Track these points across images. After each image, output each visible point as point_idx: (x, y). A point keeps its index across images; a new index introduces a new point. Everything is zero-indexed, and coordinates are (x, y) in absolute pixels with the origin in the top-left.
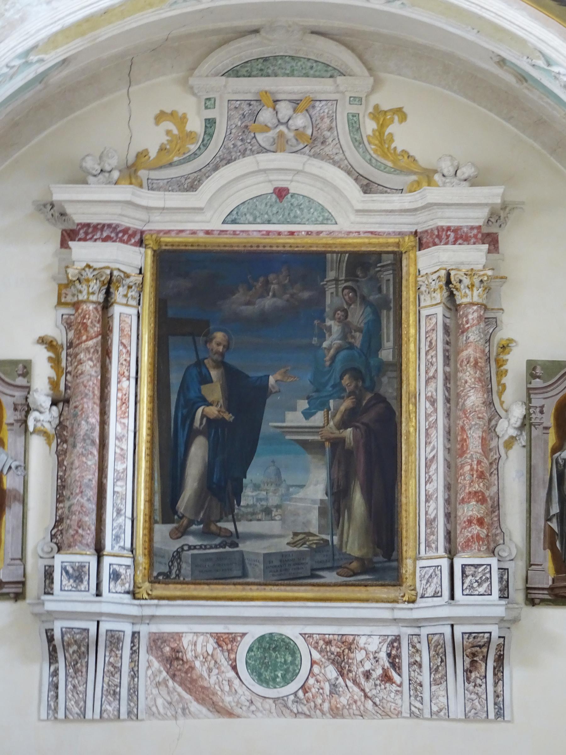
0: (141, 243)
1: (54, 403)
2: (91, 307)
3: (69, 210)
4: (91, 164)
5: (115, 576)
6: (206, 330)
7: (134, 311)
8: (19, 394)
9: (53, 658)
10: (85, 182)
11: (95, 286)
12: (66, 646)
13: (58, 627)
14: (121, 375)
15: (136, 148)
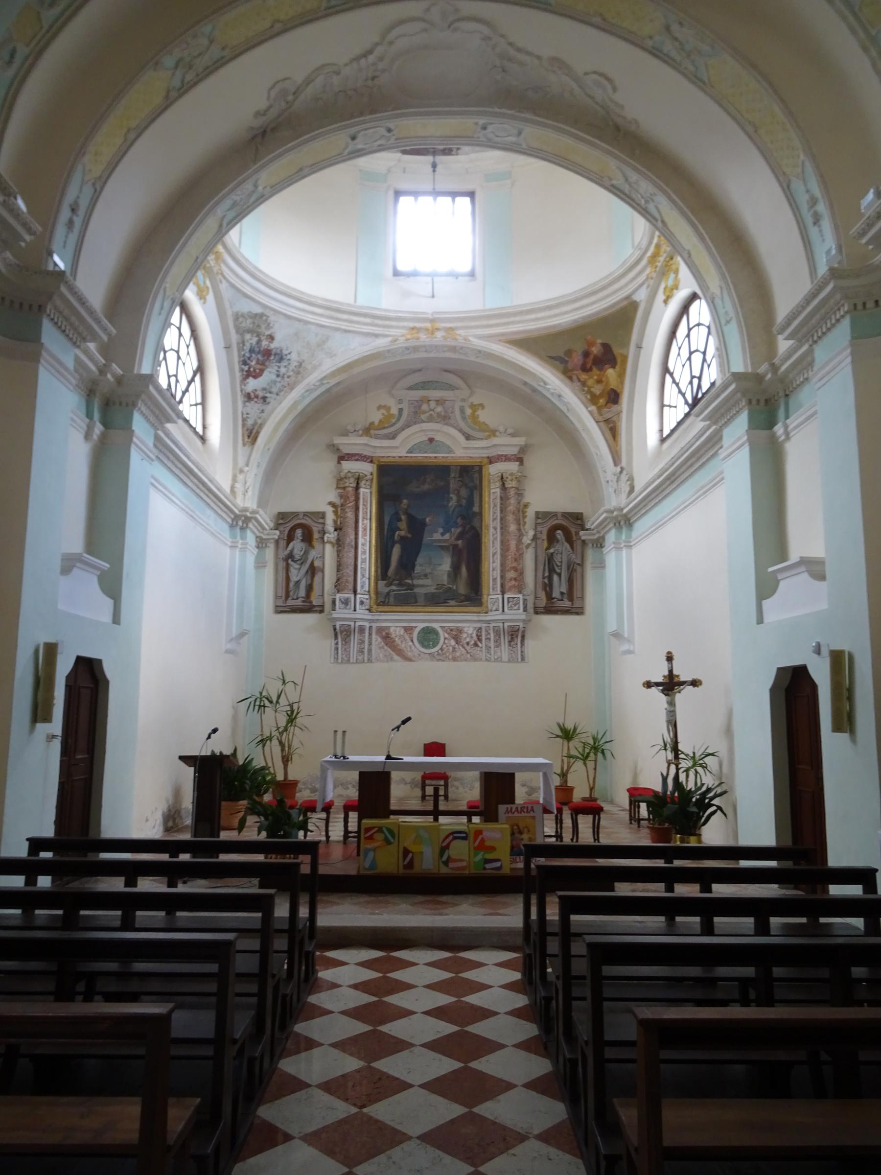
1: (336, 530)
2: (351, 489)
3: (341, 447)
4: (350, 428)
5: (362, 603)
7: (368, 491)
9: (336, 637)
10: (347, 435)
11: (352, 480)
13: (338, 624)
14: (364, 518)
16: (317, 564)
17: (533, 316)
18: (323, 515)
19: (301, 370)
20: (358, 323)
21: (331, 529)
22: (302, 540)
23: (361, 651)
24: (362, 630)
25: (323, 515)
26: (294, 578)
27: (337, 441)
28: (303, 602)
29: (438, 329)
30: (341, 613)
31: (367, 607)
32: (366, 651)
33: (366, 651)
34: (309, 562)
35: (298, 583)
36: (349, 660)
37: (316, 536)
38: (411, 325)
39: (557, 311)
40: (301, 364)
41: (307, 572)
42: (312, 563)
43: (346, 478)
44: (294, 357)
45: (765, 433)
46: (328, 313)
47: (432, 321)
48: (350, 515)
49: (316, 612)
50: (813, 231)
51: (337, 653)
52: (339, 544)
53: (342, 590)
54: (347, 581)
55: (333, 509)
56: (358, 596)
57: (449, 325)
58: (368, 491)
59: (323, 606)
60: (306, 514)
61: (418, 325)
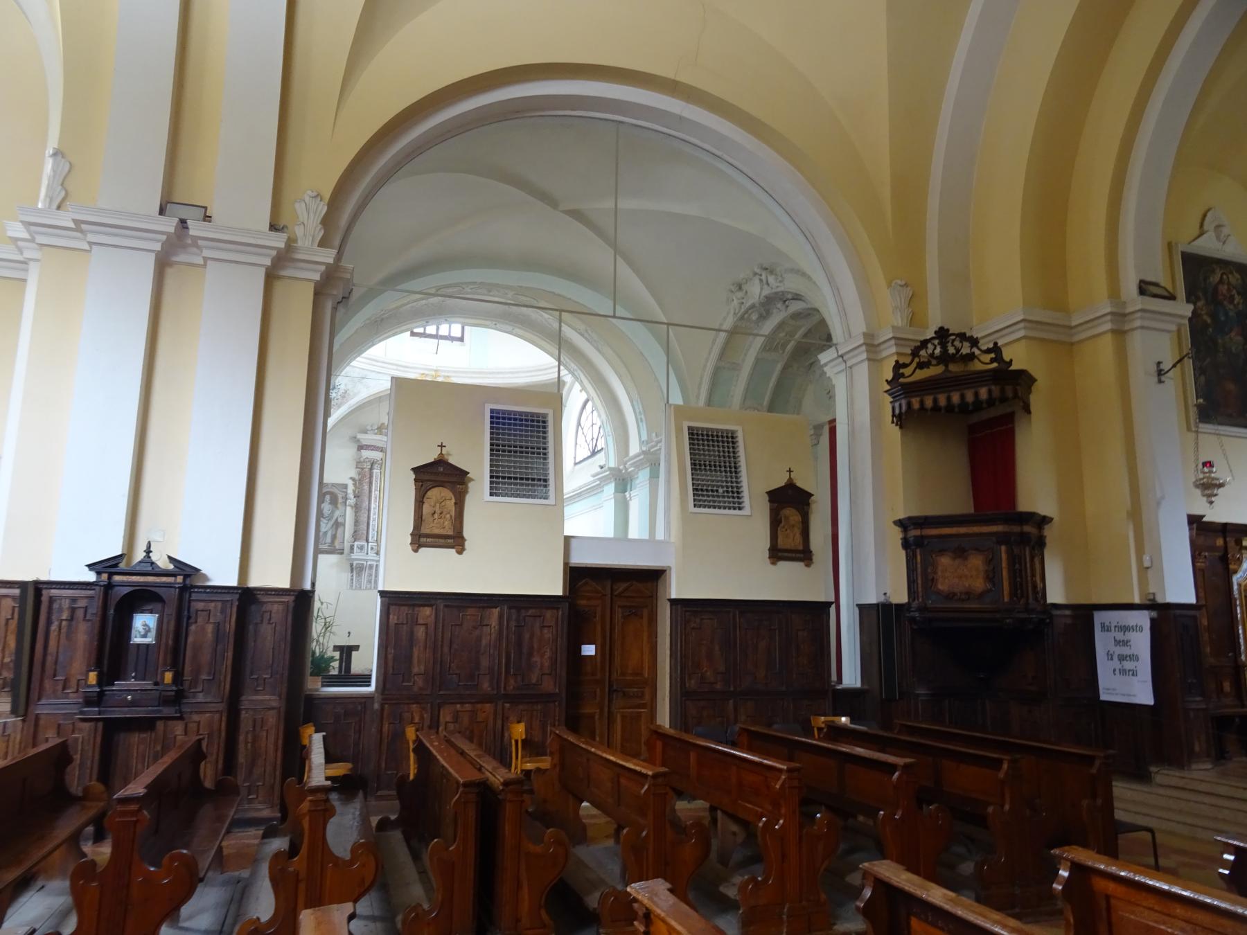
0: (381, 451)
1: (355, 497)
2: (367, 470)
3: (362, 440)
4: (369, 428)
5: (372, 548)
6: (803, 340)
7: (379, 471)
8: (344, 494)
9: (352, 571)
10: (367, 433)
11: (369, 464)
12: (356, 568)
13: (355, 563)
14: (375, 490)
15: (381, 422)
16: (340, 520)
17: (501, 376)
18: (345, 486)
19: (346, 395)
20: (389, 369)
21: (352, 496)
22: (330, 503)
23: (370, 582)
24: (371, 567)
25: (345, 486)
26: (323, 529)
27: (360, 436)
28: (329, 546)
29: (439, 376)
30: (357, 555)
31: (376, 551)
32: (373, 581)
33: (373, 581)
34: (335, 518)
35: (326, 533)
36: (361, 587)
37: (340, 500)
38: (422, 372)
39: (516, 375)
40: (346, 392)
41: (333, 526)
42: (337, 519)
43: (364, 462)
44: (342, 387)
45: (622, 494)
46: (368, 361)
47: (436, 371)
48: (366, 487)
49: (338, 553)
50: (641, 424)
51: (352, 583)
52: (357, 508)
53: (359, 539)
54: (362, 533)
55: (353, 482)
56: (370, 544)
57: (446, 374)
58: (379, 471)
59: (343, 550)
60: (333, 485)
61: (426, 372)
